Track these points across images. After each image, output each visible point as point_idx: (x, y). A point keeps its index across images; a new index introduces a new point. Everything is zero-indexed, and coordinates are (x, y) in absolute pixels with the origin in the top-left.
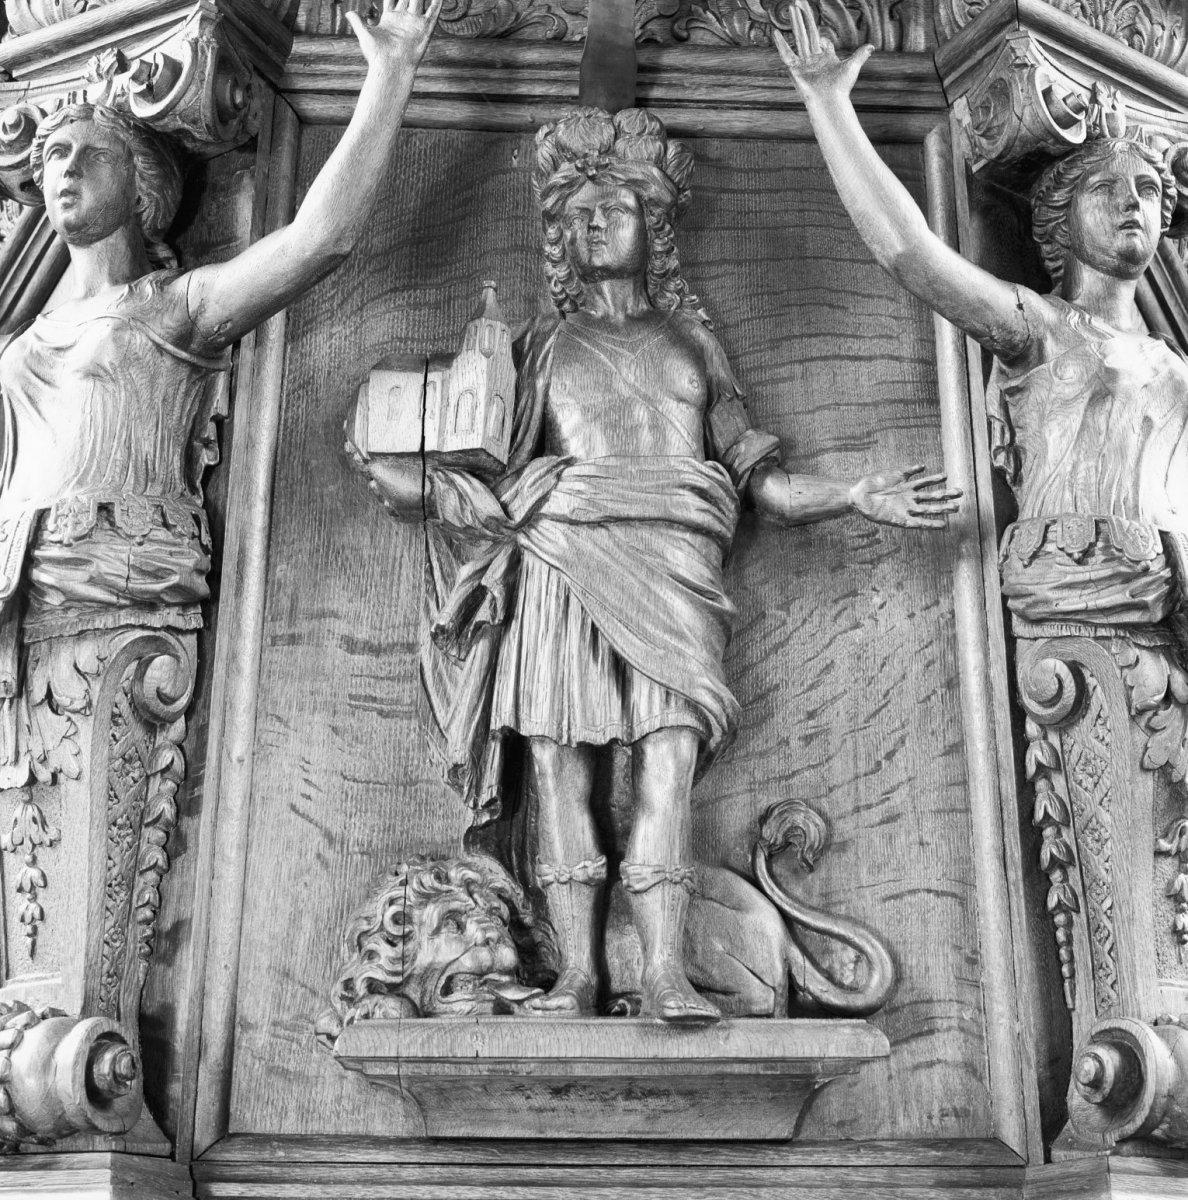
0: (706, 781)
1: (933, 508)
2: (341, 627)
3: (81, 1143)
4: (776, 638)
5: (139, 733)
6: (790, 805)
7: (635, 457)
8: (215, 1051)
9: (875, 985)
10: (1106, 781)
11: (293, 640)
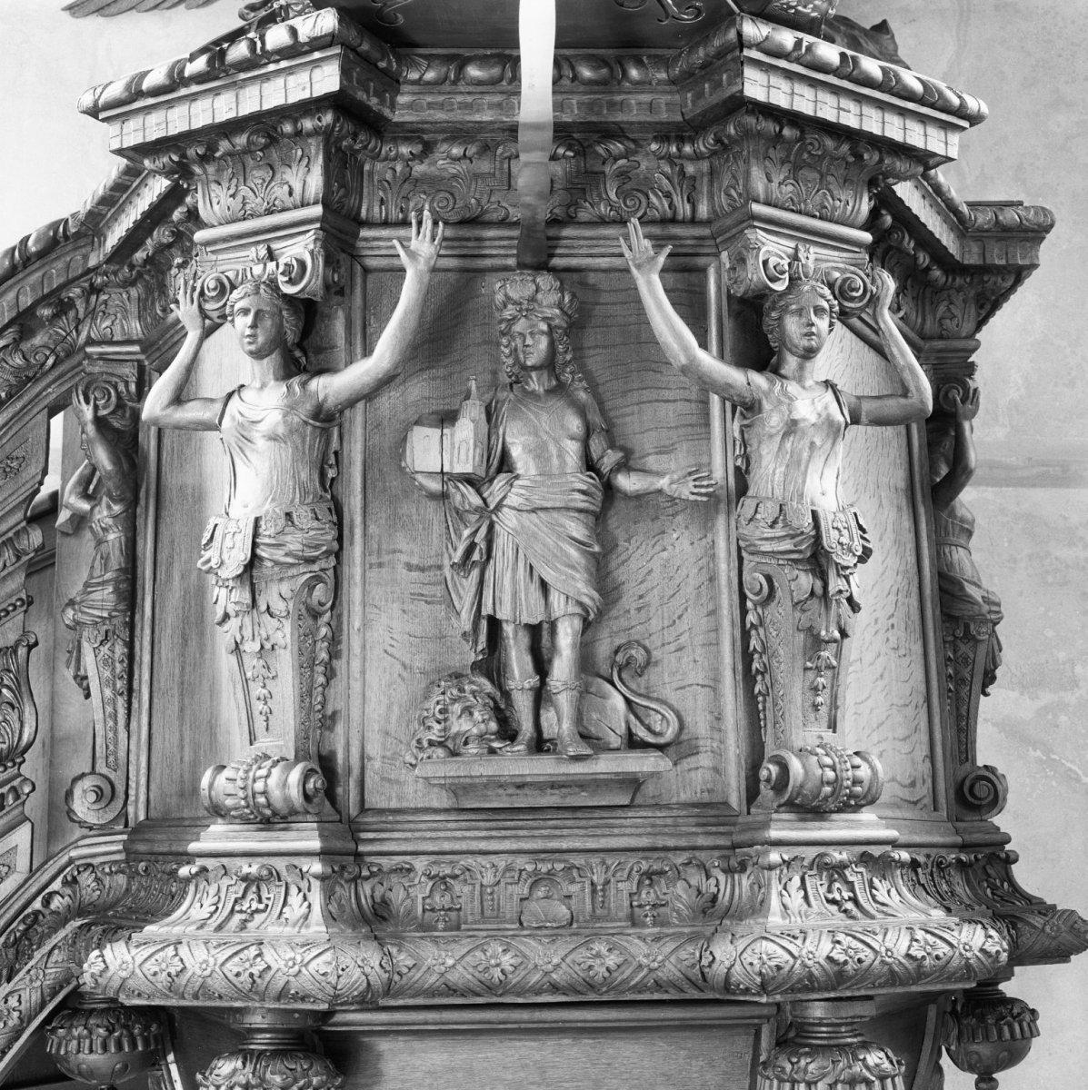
0: (589, 633)
1: (703, 490)
2: (404, 558)
3: (300, 818)
4: (623, 557)
5: (310, 621)
6: (629, 645)
7: (550, 476)
8: (356, 772)
9: (669, 734)
10: (782, 634)
11: (380, 565)
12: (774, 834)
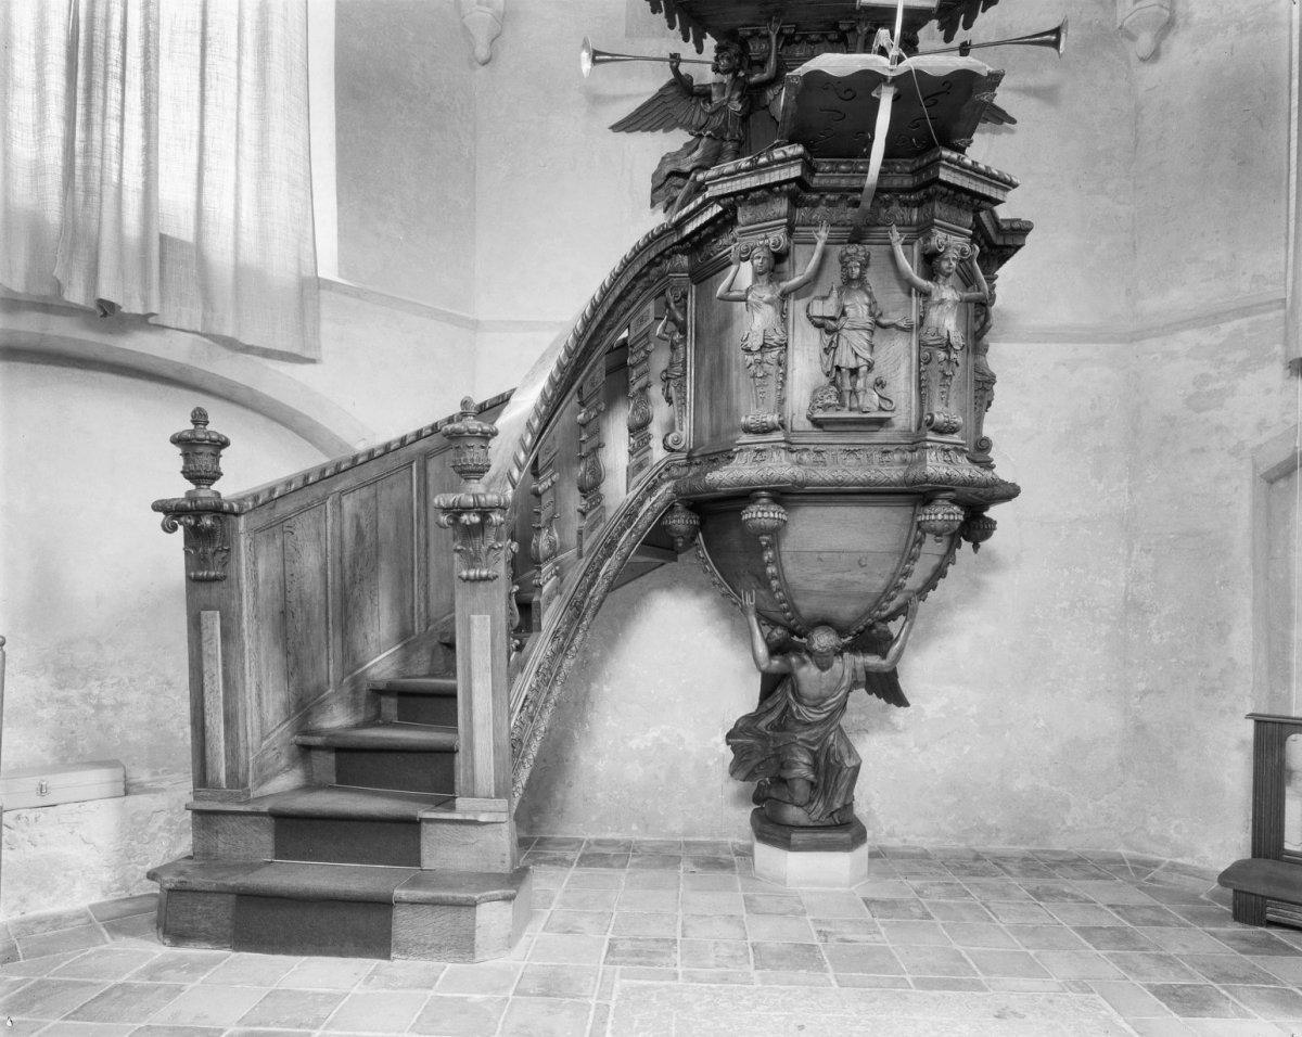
12: (928, 437)
